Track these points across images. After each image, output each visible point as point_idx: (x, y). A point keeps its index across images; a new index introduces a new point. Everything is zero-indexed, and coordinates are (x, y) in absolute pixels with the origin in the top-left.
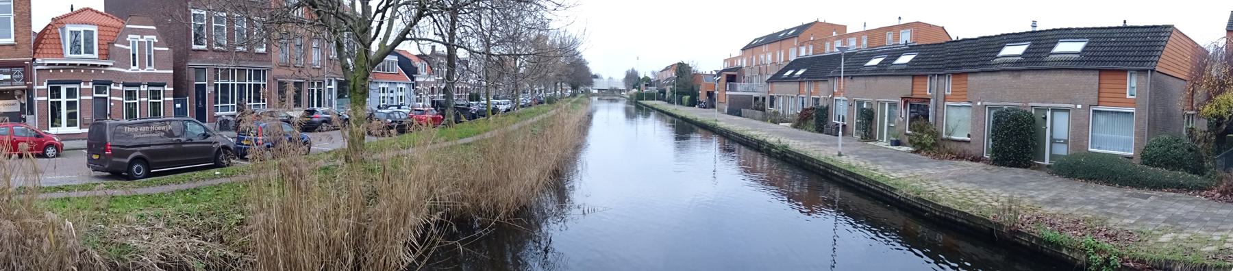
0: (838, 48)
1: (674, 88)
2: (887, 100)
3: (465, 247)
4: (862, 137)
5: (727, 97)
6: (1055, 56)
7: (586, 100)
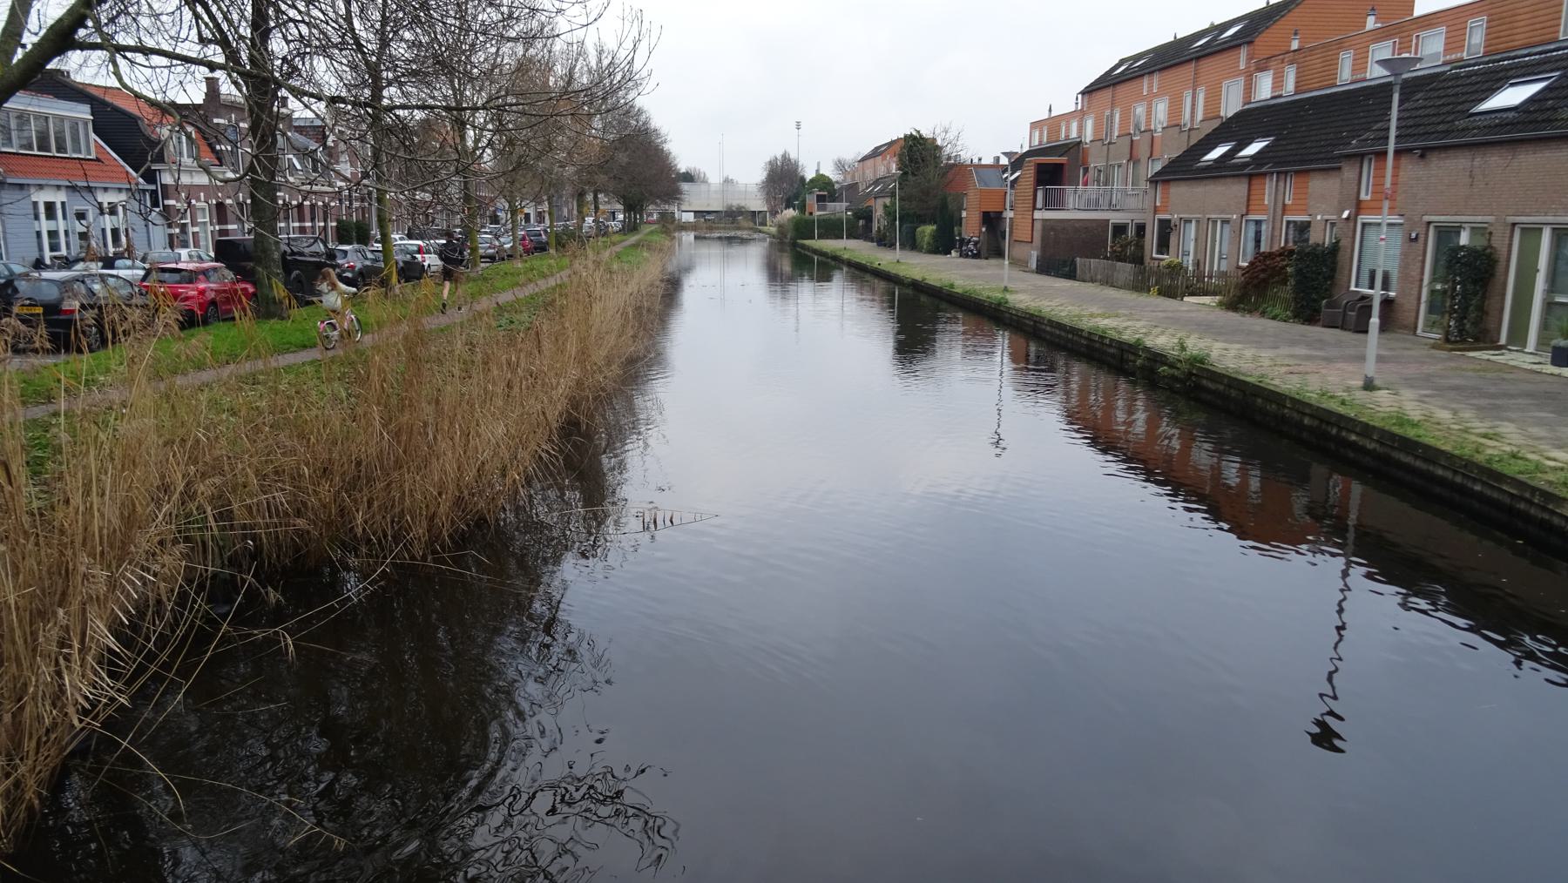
0: (1383, 63)
1: (893, 204)
2: (1550, 219)
3: (296, 640)
4: (1447, 333)
5: (1038, 226)
7: (658, 239)
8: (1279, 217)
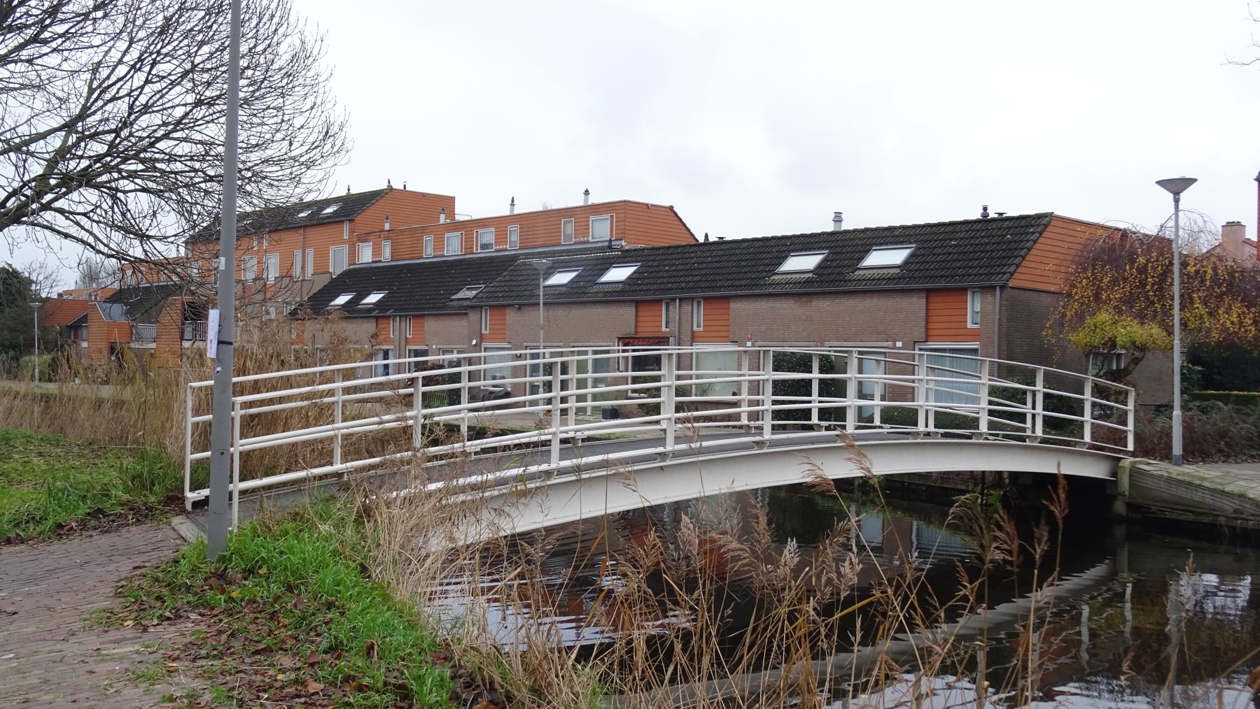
2: (456, 346)
6: (865, 272)
8: (403, 348)
